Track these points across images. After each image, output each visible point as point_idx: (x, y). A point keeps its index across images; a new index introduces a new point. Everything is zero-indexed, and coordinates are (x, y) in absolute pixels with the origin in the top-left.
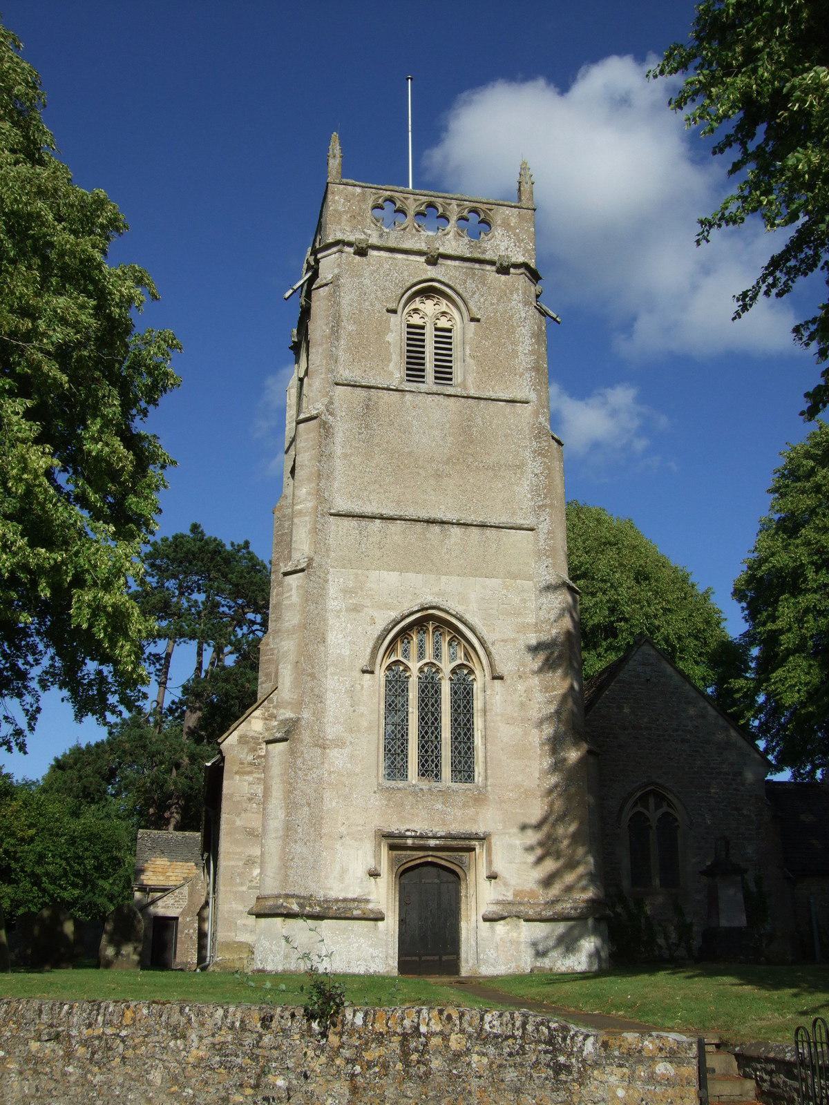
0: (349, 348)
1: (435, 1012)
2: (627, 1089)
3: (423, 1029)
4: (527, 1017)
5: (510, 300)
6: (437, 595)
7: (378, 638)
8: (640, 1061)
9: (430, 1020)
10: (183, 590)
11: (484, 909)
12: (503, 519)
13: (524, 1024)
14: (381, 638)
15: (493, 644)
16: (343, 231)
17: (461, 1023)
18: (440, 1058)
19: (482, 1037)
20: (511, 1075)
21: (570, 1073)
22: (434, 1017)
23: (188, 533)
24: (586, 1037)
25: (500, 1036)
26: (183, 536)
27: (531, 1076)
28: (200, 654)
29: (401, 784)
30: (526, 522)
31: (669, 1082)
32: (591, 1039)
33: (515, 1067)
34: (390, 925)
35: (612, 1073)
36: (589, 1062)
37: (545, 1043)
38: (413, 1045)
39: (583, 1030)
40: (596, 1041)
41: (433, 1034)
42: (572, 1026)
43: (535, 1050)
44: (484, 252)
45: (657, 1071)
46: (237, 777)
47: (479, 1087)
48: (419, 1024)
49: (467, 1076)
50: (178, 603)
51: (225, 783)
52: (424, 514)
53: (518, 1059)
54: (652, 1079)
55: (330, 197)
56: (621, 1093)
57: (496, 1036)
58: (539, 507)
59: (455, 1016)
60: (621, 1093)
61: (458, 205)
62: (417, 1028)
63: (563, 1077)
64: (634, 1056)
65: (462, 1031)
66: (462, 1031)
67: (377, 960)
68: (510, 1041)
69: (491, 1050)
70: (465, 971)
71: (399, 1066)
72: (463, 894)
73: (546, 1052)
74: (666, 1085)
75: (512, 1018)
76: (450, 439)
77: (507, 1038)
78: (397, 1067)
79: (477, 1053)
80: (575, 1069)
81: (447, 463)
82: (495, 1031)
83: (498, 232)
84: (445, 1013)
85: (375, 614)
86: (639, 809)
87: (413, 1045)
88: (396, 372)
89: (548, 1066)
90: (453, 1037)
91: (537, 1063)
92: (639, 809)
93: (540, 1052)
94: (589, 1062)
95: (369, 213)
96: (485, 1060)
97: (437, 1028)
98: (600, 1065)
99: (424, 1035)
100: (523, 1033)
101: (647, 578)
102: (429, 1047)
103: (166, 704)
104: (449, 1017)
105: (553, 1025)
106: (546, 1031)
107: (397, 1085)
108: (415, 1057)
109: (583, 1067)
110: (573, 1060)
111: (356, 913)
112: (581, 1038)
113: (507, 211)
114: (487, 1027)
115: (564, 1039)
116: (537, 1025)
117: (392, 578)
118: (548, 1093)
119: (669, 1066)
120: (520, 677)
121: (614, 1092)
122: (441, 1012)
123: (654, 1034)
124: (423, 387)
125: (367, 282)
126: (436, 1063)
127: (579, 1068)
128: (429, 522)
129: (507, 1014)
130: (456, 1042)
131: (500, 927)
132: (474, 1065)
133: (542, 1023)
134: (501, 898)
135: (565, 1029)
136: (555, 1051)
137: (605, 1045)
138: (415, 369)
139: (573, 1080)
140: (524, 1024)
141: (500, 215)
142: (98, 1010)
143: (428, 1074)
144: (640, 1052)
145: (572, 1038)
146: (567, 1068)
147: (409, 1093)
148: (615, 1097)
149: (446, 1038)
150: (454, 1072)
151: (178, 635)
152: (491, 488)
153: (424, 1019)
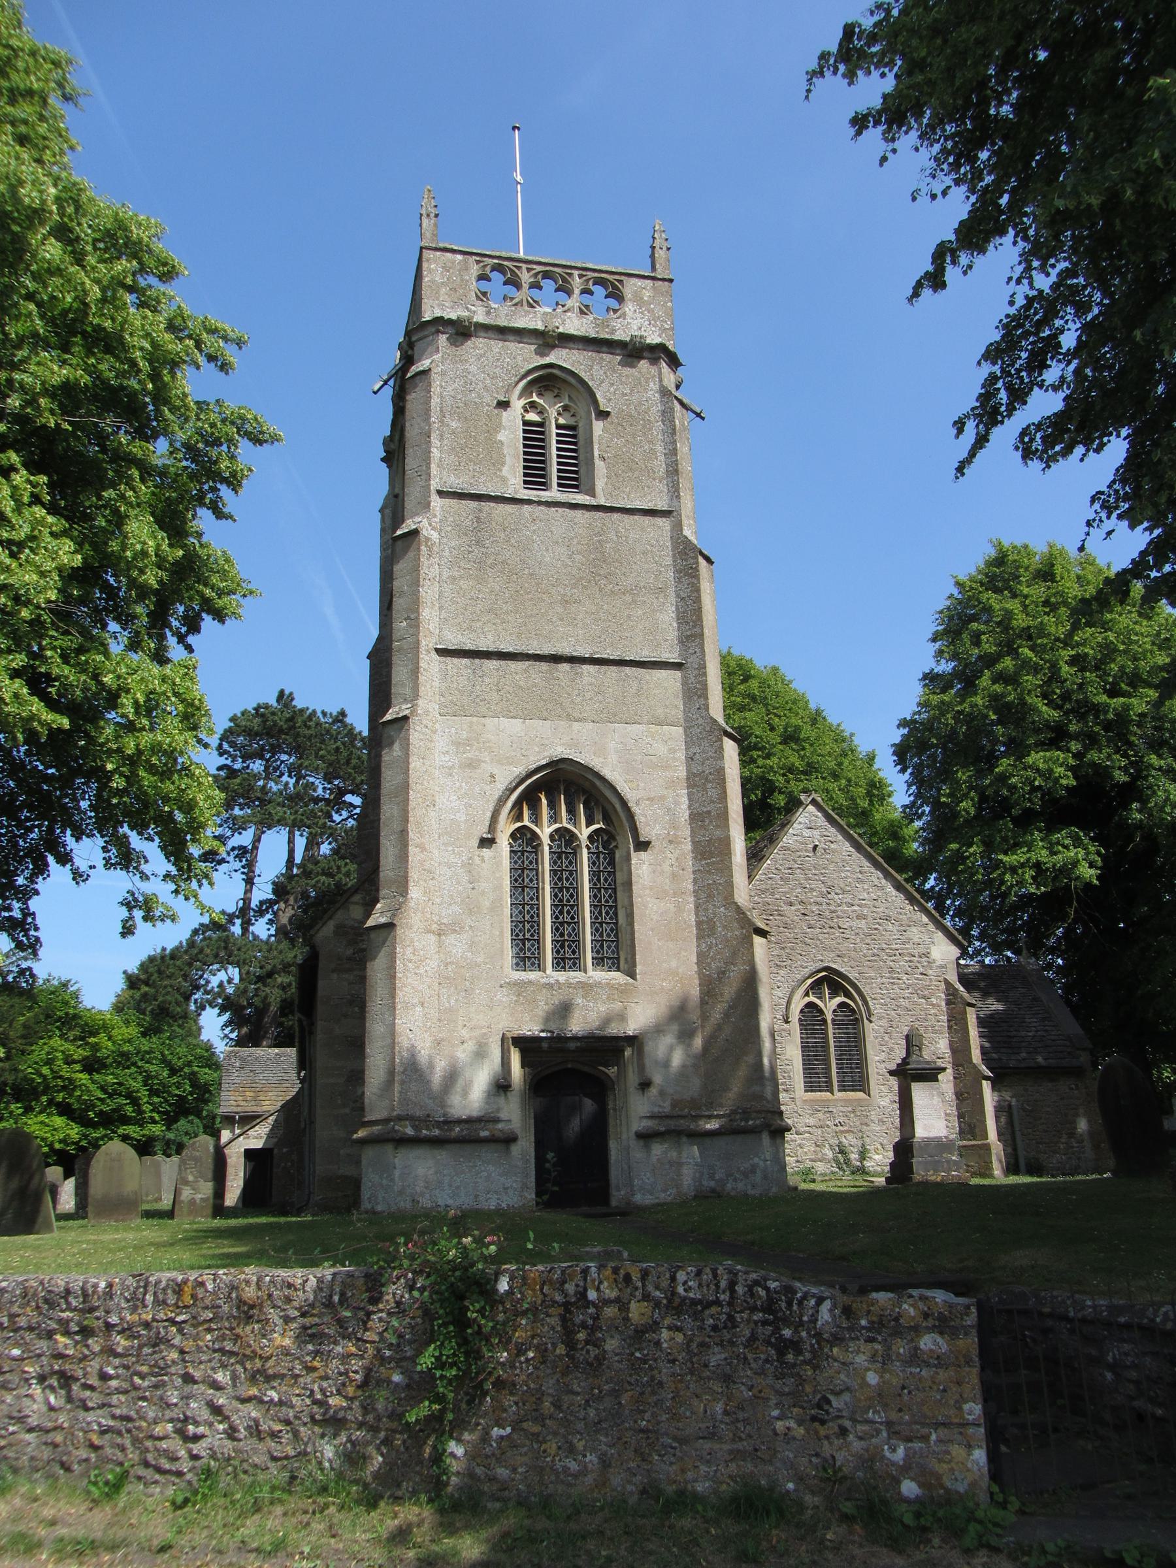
0: (453, 449)
1: (609, 1272)
2: (881, 1373)
3: (592, 1295)
4: (736, 1275)
5: (646, 390)
6: (570, 746)
7: (500, 800)
8: (897, 1333)
9: (601, 1282)
10: (270, 772)
11: (637, 1125)
12: (645, 655)
13: (732, 1285)
14: (501, 801)
15: (637, 804)
16: (442, 306)
17: (644, 1285)
18: (617, 1336)
19: (675, 1305)
20: (716, 1357)
21: (799, 1352)
22: (607, 1279)
23: (273, 702)
24: (820, 1301)
25: (700, 1302)
26: (267, 707)
27: (745, 1358)
28: (291, 841)
29: (533, 976)
30: (674, 657)
31: (940, 1361)
32: (827, 1304)
33: (722, 1346)
34: (525, 1147)
35: (858, 1352)
36: (826, 1336)
37: (763, 1310)
38: (579, 1318)
39: (814, 1290)
40: (834, 1306)
41: (608, 1302)
42: (797, 1284)
43: (749, 1321)
44: (613, 331)
45: (922, 1346)
46: (335, 976)
47: (673, 1375)
48: (585, 1290)
49: (655, 1360)
50: (264, 786)
51: (321, 984)
52: (548, 649)
53: (726, 1335)
54: (915, 1358)
55: (425, 265)
56: (872, 1378)
57: (694, 1302)
58: (687, 637)
59: (636, 1276)
60: (872, 1378)
61: (581, 276)
62: (583, 1295)
63: (790, 1357)
64: (887, 1327)
65: (646, 1297)
66: (646, 1297)
67: (511, 1192)
68: (714, 1310)
69: (687, 1321)
70: (617, 1197)
71: (561, 1350)
72: (611, 1106)
73: (765, 1323)
74: (935, 1366)
75: (715, 1275)
76: (578, 557)
77: (709, 1304)
78: (558, 1351)
79: (669, 1328)
80: (807, 1346)
81: (574, 586)
82: (691, 1295)
83: (629, 308)
84: (622, 1272)
85: (495, 771)
86: (812, 998)
87: (579, 1318)
88: (512, 481)
89: (769, 1343)
90: (633, 1305)
91: (753, 1338)
92: (812, 998)
93: (756, 1323)
94: (826, 1336)
95: (474, 285)
96: (679, 1338)
97: (610, 1293)
98: (842, 1339)
99: (593, 1303)
100: (732, 1297)
101: (797, 740)
102: (602, 1322)
103: (254, 903)
104: (628, 1278)
105: (773, 1285)
106: (762, 1293)
107: (558, 1376)
108: (581, 1336)
109: (818, 1342)
110: (804, 1334)
111: (484, 1134)
112: (813, 1302)
113: (640, 283)
114: (680, 1290)
115: (789, 1304)
116: (750, 1289)
117: (515, 726)
118: (770, 1380)
119: (939, 1340)
120: (671, 842)
121: (863, 1379)
122: (616, 1271)
123: (915, 1292)
124: (545, 495)
125: (473, 369)
126: (612, 1344)
127: (812, 1345)
128: (556, 659)
129: (708, 1270)
130: (637, 1311)
131: (658, 1149)
132: (665, 1345)
133: (756, 1283)
134: (656, 1109)
135: (789, 1290)
136: (778, 1321)
137: (847, 1311)
138: (535, 474)
139: (805, 1362)
140: (732, 1285)
141: (630, 287)
142: (145, 1287)
143: (600, 1359)
144: (896, 1319)
145: (800, 1303)
146: (795, 1345)
147: (576, 1388)
148: (864, 1384)
149: (624, 1307)
150: (638, 1355)
151: (266, 823)
152: (629, 617)
153: (593, 1281)
